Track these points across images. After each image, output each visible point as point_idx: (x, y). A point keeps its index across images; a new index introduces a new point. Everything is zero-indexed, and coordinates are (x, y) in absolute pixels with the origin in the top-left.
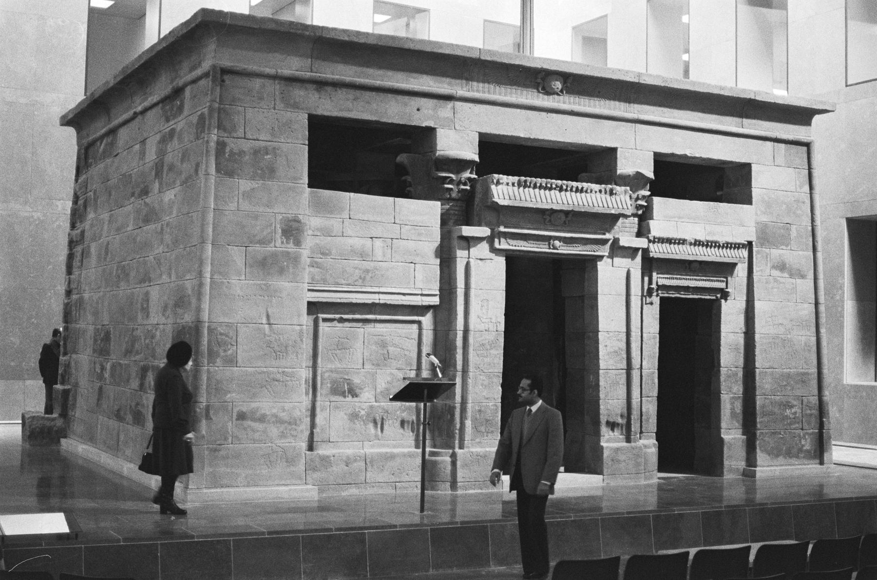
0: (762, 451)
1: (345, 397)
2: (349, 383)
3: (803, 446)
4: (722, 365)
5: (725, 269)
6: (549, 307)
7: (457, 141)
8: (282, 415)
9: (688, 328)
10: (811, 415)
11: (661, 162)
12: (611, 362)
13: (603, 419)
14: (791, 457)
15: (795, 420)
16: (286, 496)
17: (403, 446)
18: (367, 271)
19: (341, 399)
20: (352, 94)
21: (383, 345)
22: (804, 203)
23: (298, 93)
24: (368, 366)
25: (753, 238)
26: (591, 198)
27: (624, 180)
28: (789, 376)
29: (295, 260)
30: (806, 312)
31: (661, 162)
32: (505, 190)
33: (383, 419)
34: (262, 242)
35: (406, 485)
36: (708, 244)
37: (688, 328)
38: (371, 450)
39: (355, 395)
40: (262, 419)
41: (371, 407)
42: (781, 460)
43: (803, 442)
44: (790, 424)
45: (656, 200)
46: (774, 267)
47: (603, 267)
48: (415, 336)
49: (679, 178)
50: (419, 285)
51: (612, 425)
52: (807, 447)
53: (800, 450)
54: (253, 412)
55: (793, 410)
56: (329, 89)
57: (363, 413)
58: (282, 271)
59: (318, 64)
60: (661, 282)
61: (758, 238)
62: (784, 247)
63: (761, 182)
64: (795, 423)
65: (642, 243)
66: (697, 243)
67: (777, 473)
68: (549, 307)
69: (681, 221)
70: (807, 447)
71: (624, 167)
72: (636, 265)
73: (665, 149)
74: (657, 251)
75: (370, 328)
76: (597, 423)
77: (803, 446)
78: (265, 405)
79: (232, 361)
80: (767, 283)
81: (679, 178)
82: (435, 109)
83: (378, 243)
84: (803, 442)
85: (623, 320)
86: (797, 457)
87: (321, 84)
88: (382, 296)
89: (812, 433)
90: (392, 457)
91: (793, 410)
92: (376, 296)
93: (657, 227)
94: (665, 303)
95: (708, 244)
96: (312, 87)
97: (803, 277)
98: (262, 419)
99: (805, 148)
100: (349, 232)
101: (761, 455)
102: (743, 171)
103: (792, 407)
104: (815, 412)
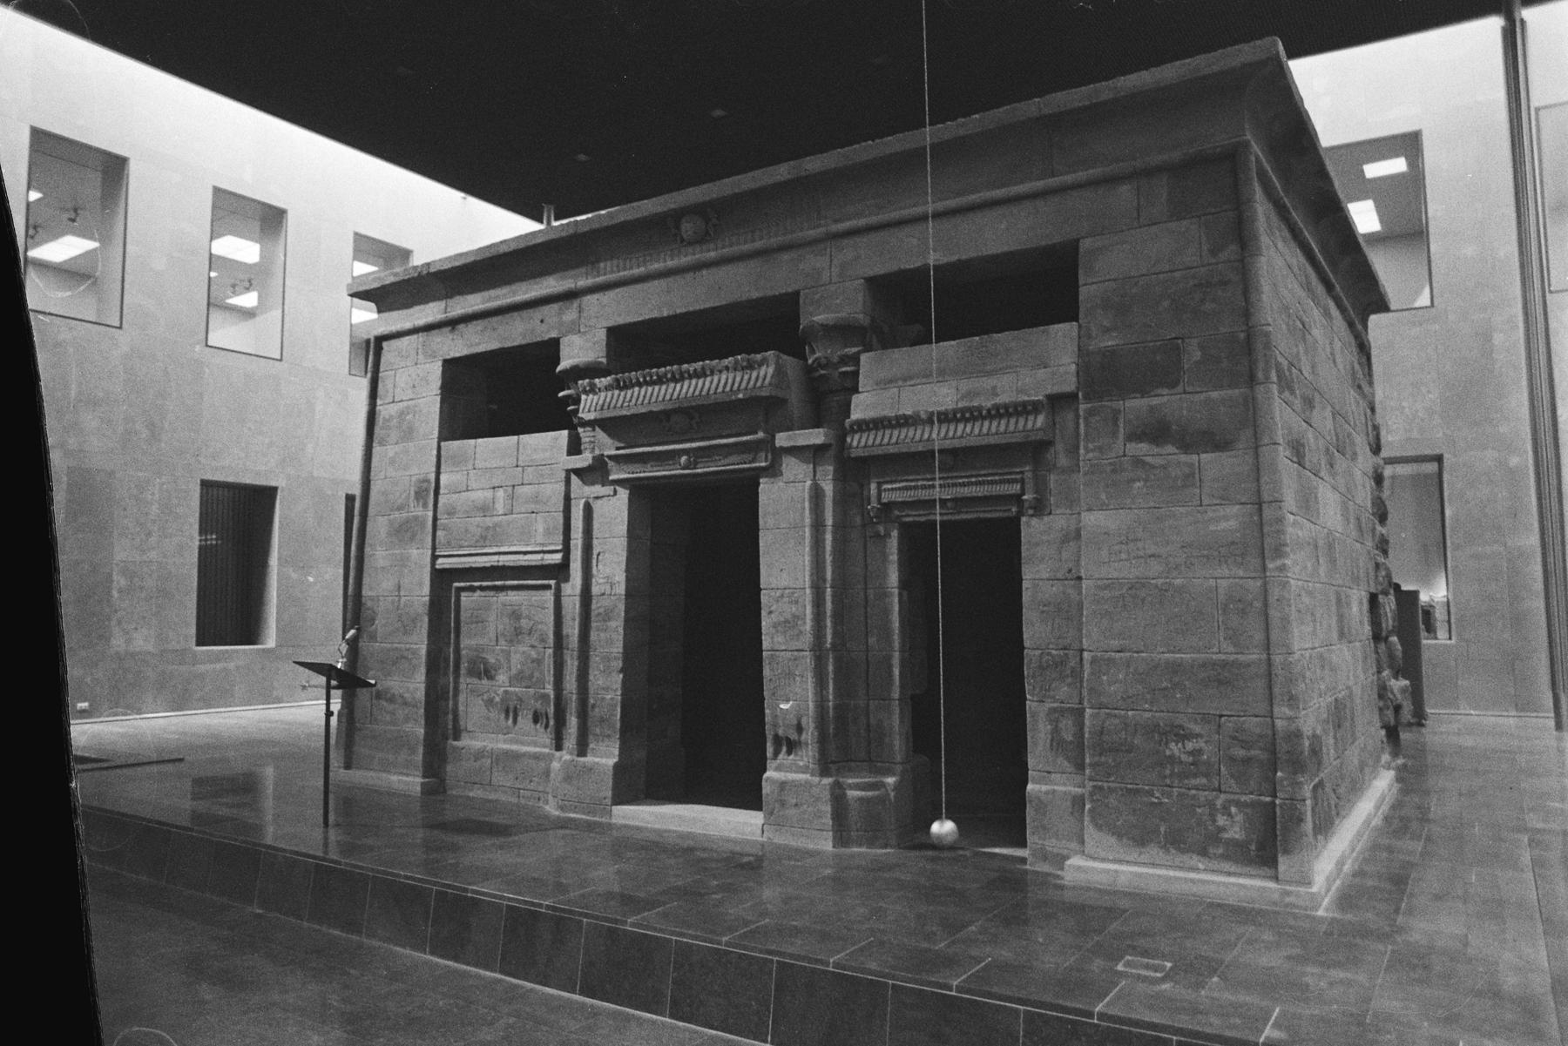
0: (1099, 827)
2: (485, 662)
3: (1222, 829)
4: (1027, 644)
10: (1247, 761)
12: (780, 639)
14: (1183, 851)
16: (396, 786)
17: (535, 744)
18: (488, 528)
19: (475, 681)
21: (516, 615)
24: (502, 642)
25: (1069, 386)
28: (1175, 668)
30: (1233, 524)
31: (880, 287)
34: (400, 508)
35: (528, 794)
38: (502, 745)
39: (491, 678)
40: (392, 700)
41: (506, 692)
42: (1153, 852)
43: (1221, 820)
44: (1184, 775)
46: (1133, 437)
48: (551, 605)
50: (540, 539)
52: (1235, 833)
53: (1215, 837)
54: (387, 691)
55: (1190, 746)
57: (497, 699)
62: (1166, 391)
64: (1195, 776)
66: (945, 418)
67: (1122, 880)
70: (1235, 833)
74: (858, 443)
75: (503, 597)
77: (1222, 829)
78: (394, 684)
80: (1114, 471)
82: (560, 313)
83: (500, 493)
84: (1221, 820)
86: (1203, 853)
88: (502, 558)
89: (1252, 805)
90: (517, 756)
91: (1190, 746)
92: (496, 558)
93: (862, 407)
96: (446, 330)
98: (392, 700)
100: (473, 485)
101: (1097, 835)
103: (1184, 737)
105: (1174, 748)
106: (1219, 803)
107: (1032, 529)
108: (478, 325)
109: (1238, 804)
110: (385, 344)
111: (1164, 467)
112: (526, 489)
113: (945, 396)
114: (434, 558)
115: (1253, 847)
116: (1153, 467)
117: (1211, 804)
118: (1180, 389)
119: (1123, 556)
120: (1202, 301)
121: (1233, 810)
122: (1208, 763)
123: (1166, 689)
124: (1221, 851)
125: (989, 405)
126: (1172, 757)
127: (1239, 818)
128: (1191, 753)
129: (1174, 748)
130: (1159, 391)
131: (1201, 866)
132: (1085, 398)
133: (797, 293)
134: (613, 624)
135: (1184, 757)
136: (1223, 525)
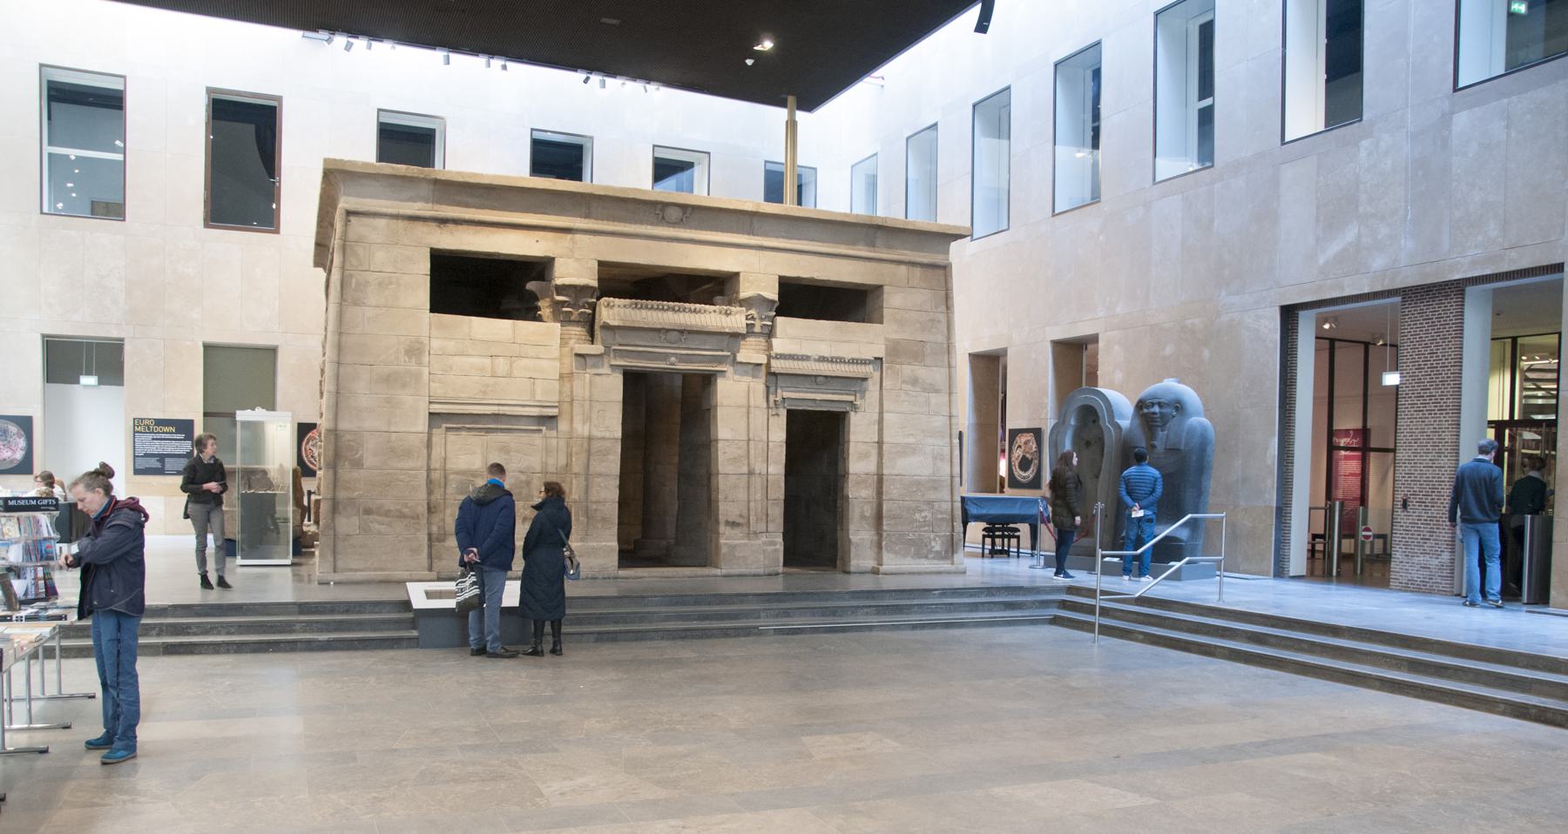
5: (855, 383)
6: (665, 418)
7: (575, 265)
8: (406, 510)
9: (815, 440)
11: (786, 285)
13: (722, 518)
15: (925, 523)
20: (472, 229)
23: (420, 228)
26: (710, 317)
27: (747, 303)
29: (418, 377)
31: (786, 285)
32: (613, 311)
36: (832, 360)
37: (815, 440)
45: (779, 319)
47: (722, 386)
49: (801, 299)
50: (538, 397)
51: (734, 524)
52: (937, 548)
56: (451, 226)
58: (404, 386)
59: (436, 207)
60: (786, 395)
61: (887, 354)
63: (893, 301)
65: (763, 359)
66: (822, 359)
68: (665, 418)
69: (807, 341)
71: (745, 292)
72: (759, 385)
73: (577, 183)
74: (777, 365)
76: (717, 522)
79: (358, 464)
81: (801, 299)
85: (746, 437)
87: (443, 221)
93: (778, 345)
94: (792, 415)
95: (832, 360)
96: (434, 225)
97: (937, 391)
99: (941, 272)
102: (538, 167)
108: (550, 235)
110: (353, 219)
112: (524, 362)
113: (825, 350)
134: (611, 457)
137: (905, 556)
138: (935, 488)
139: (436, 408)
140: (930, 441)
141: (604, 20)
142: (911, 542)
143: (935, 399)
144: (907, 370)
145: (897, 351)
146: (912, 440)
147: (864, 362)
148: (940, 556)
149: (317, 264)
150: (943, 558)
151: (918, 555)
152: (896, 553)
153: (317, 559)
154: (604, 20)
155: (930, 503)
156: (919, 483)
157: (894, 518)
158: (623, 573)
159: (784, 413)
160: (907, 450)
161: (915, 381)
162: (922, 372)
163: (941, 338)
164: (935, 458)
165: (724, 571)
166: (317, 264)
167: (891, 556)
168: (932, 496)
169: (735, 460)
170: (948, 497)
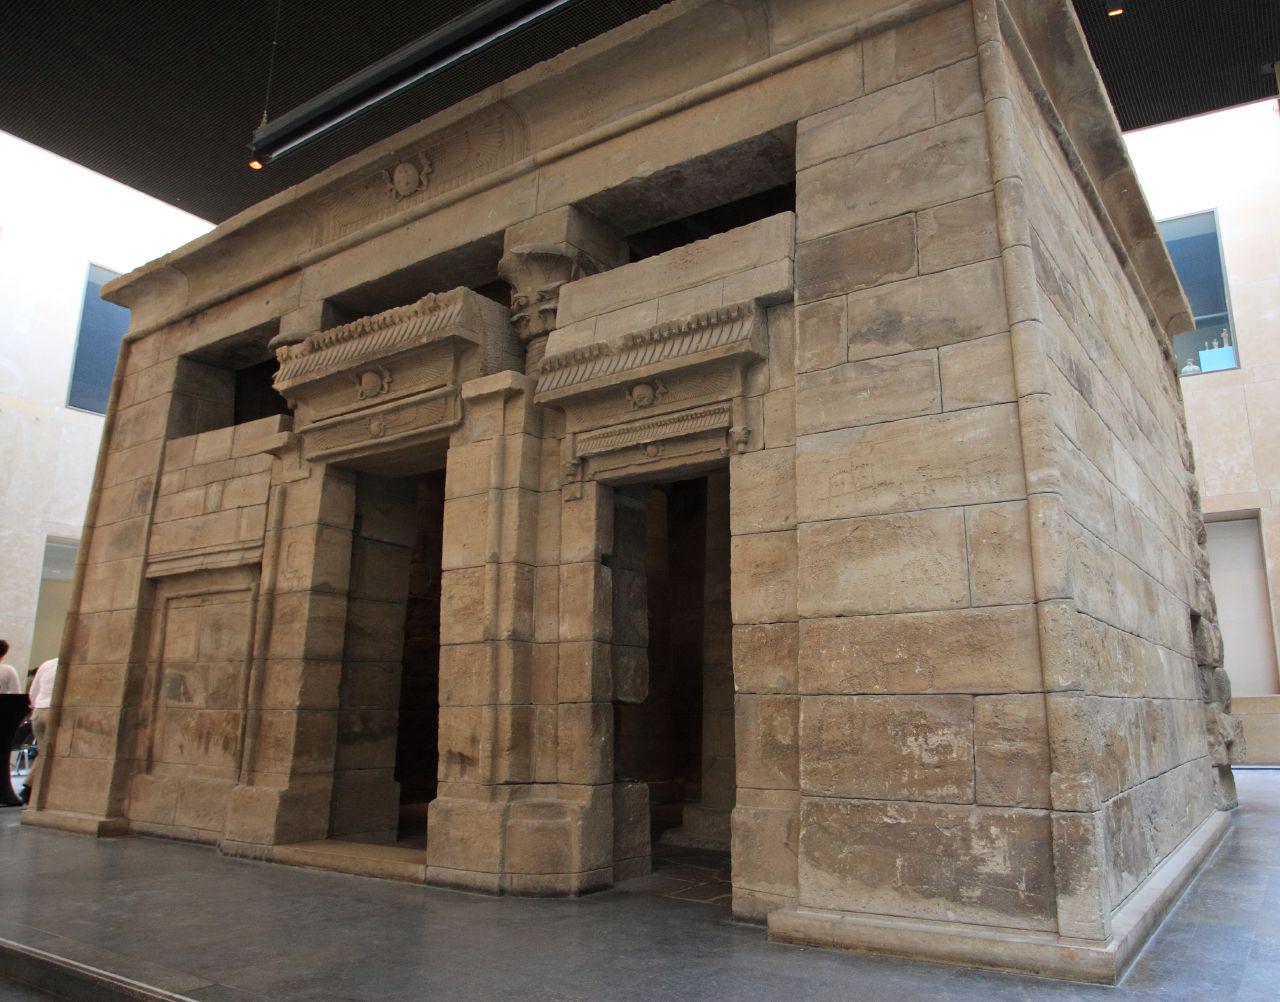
0: (816, 863)
1: (179, 700)
15: (944, 770)
22: (963, 140)
30: (982, 432)
33: (208, 733)
37: (672, 534)
44: (926, 783)
52: (997, 864)
55: (934, 740)
62: (896, 276)
63: (817, 154)
64: (942, 781)
66: (634, 343)
74: (551, 387)
77: (979, 860)
84: (978, 847)
91: (934, 740)
103: (926, 730)
104: (1034, 749)
105: (913, 745)
106: (973, 820)
107: (742, 472)
109: (999, 821)
111: (895, 368)
113: (642, 320)
114: (147, 564)
115: (1022, 886)
116: (882, 371)
117: (966, 829)
118: (913, 271)
119: (846, 488)
120: (938, 165)
121: (994, 831)
122: (959, 763)
123: (902, 662)
124: (978, 893)
125: (689, 318)
126: (910, 756)
127: (1002, 842)
128: (936, 751)
129: (913, 745)
130: (885, 278)
131: (951, 916)
132: (802, 298)
133: (792, 127)
135: (927, 758)
136: (971, 434)
137: (872, 884)
138: (977, 649)
139: (155, 571)
140: (948, 493)
141: (1120, 12)
142: (895, 838)
143: (957, 360)
144: (863, 302)
145: (826, 268)
146: (887, 500)
147: (727, 318)
148: (1000, 896)
149: (80, 396)
150: (1019, 908)
151: (919, 883)
152: (842, 870)
153: (484, 806)
154: (1120, 12)
155: (962, 701)
156: (914, 635)
157: (833, 751)
158: (279, 851)
159: (591, 489)
160: (865, 534)
161: (888, 327)
162: (908, 295)
163: (969, 182)
164: (970, 545)
165: (432, 872)
166: (80, 396)
167: (827, 878)
168: (965, 674)
169: (469, 611)
170: (1028, 678)
